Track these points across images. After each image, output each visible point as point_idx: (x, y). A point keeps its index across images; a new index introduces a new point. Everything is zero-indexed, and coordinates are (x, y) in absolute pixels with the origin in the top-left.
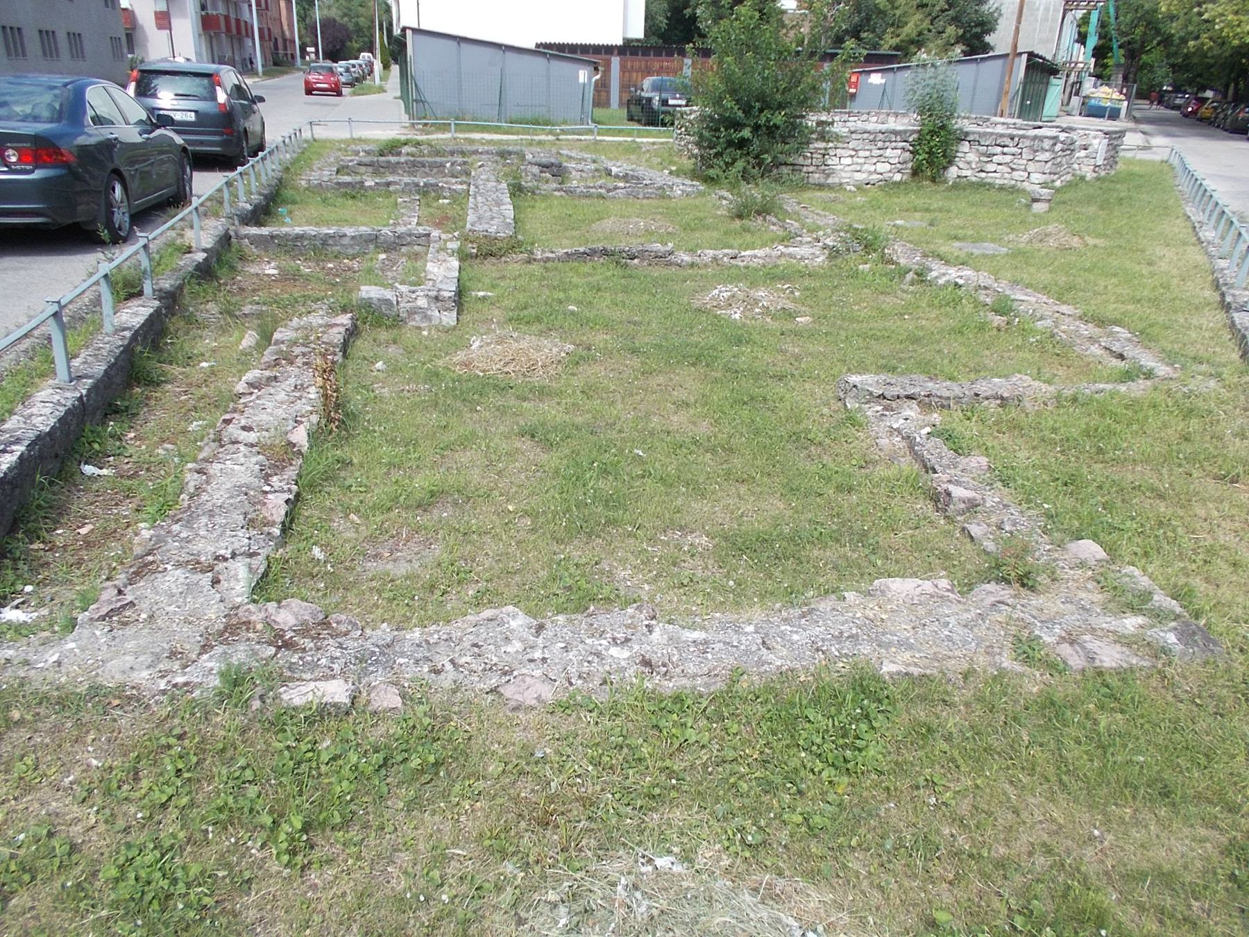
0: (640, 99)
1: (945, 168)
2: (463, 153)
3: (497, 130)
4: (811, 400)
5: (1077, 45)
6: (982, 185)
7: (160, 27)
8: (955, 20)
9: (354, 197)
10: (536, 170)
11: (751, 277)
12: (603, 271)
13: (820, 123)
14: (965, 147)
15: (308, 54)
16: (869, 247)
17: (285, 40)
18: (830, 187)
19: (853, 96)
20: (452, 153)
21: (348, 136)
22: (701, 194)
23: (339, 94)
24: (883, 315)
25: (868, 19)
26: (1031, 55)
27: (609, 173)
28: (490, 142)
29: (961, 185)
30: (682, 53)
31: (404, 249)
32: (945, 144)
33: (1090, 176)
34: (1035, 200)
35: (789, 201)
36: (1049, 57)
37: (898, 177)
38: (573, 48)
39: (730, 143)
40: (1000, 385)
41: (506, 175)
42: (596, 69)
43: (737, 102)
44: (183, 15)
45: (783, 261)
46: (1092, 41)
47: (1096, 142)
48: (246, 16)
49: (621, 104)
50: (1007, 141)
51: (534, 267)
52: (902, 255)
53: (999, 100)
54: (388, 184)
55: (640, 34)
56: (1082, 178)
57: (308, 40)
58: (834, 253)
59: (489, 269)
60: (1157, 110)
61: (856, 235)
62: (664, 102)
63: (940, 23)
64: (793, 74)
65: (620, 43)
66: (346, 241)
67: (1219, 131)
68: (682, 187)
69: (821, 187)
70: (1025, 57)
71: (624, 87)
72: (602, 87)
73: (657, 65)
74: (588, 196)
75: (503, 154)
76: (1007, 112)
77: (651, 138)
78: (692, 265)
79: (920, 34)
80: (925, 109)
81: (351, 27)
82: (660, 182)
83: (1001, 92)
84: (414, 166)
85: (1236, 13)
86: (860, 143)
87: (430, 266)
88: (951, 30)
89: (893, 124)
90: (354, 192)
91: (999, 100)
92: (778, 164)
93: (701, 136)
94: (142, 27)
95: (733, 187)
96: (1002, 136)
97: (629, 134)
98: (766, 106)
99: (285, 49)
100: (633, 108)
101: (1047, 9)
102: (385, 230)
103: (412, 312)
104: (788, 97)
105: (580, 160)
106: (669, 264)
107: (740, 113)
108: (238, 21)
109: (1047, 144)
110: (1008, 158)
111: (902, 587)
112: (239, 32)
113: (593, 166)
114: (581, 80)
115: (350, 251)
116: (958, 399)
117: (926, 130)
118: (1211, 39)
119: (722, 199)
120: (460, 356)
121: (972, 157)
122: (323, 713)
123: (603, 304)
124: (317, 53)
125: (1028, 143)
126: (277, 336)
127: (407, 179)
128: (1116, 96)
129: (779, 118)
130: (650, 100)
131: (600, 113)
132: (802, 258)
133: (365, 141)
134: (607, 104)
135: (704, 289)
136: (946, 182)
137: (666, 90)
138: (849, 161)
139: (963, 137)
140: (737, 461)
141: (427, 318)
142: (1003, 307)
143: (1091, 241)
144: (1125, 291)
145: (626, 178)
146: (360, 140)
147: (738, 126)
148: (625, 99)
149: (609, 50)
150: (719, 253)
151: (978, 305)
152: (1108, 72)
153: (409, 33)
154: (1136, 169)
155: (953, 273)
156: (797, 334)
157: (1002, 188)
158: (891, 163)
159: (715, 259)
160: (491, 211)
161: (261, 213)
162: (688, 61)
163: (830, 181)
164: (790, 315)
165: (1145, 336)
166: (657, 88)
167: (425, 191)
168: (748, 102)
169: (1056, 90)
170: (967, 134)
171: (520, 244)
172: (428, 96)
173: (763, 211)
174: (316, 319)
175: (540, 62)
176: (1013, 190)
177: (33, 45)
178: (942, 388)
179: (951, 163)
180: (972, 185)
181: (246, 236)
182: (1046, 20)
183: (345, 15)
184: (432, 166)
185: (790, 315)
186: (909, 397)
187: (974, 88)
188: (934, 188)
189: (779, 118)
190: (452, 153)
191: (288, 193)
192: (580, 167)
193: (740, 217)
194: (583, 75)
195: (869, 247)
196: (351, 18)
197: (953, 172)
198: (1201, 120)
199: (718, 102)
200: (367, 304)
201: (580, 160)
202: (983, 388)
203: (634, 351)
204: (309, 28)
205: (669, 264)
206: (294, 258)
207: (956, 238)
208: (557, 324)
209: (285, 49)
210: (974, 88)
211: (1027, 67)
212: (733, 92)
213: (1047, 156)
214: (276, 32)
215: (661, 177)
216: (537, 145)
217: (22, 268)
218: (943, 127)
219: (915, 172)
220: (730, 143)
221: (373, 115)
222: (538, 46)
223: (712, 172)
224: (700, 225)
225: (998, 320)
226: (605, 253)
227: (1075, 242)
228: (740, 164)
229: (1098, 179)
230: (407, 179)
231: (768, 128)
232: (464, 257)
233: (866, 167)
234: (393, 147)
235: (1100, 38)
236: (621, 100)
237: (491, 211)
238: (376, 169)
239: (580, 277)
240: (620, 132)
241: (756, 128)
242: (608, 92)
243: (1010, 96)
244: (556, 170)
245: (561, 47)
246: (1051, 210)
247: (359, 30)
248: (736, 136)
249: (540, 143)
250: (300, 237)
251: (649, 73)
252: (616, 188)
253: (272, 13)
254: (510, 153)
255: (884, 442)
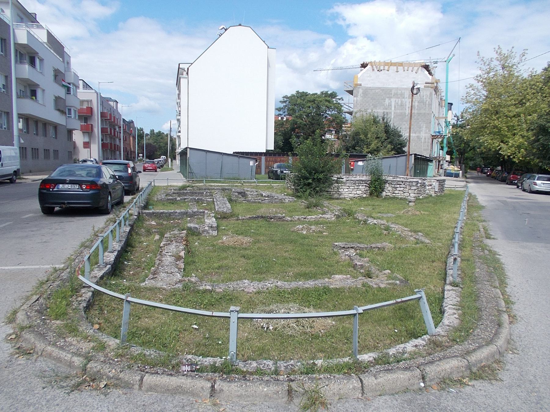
0: (273, 171)
1: (381, 192)
2: (209, 189)
3: (220, 182)
4: (325, 251)
5: (441, 151)
6: (394, 198)
7: (85, 147)
8: (391, 143)
9: (173, 204)
10: (236, 194)
11: (310, 223)
12: (261, 222)
13: (338, 178)
14: (387, 185)
15: (140, 156)
16: (349, 215)
17: (131, 152)
18: (341, 199)
19: (352, 169)
20: (205, 189)
21: (166, 185)
22: (295, 201)
23: (156, 171)
24: (352, 232)
25: (358, 143)
26: (415, 155)
27: (262, 195)
28: (220, 186)
29: (387, 198)
30: (288, 156)
31: (196, 217)
32: (380, 184)
33: (433, 195)
34: (410, 202)
35: (326, 203)
36: (428, 156)
37: (365, 196)
38: (247, 153)
39: (305, 185)
40: (379, 245)
41: (226, 196)
42: (256, 161)
43: (307, 171)
44: (95, 143)
45: (321, 219)
46: (446, 149)
47: (434, 183)
48: (118, 143)
49: (265, 173)
50: (401, 183)
51: (239, 221)
52: (360, 216)
53: (406, 170)
54: (185, 199)
55: (271, 147)
56: (431, 196)
57: (140, 151)
58: (338, 217)
59: (224, 222)
60: (475, 173)
61: (344, 210)
62: (282, 172)
63: (385, 144)
64: (325, 161)
65: (265, 151)
66: (176, 214)
67: (497, 181)
68: (288, 199)
69: (337, 199)
70: (413, 155)
71: (267, 167)
72: (259, 167)
73: (279, 159)
74: (255, 202)
75: (224, 190)
76: (409, 174)
77: (277, 184)
78: (291, 221)
79: (378, 147)
80: (372, 173)
81: (157, 146)
82: (280, 197)
83: (406, 168)
84: (192, 194)
85: (492, 140)
86: (351, 186)
87: (206, 220)
88: (389, 146)
89: (364, 178)
90: (173, 202)
91: (406, 170)
92: (321, 191)
93: (295, 182)
94: (78, 147)
95: (306, 199)
96: (399, 181)
97: (269, 182)
98: (317, 172)
99: (131, 155)
100: (270, 174)
101: (425, 139)
102: (189, 211)
103: (204, 231)
104: (324, 169)
105: (251, 192)
106: (284, 221)
107: (308, 174)
108: (115, 145)
109: (414, 184)
110: (402, 189)
111: (337, 277)
112: (115, 149)
113: (256, 193)
114: (251, 165)
115: (178, 217)
116: (366, 248)
117: (373, 180)
118: (484, 148)
119: (302, 203)
120: (220, 241)
121: (390, 188)
122: (205, 291)
123: (263, 230)
124: (143, 156)
125: (408, 183)
126: (165, 236)
127: (191, 197)
128: (456, 169)
129: (321, 176)
130: (277, 171)
131: (257, 176)
132: (328, 218)
133: (174, 186)
134: (260, 173)
135: (295, 226)
136: (382, 197)
137: (282, 168)
138: (347, 190)
139: (386, 182)
140: (301, 261)
141: (208, 233)
142: (387, 229)
143: (422, 212)
144: (428, 224)
145: (268, 196)
146: (171, 186)
147: (307, 179)
148: (267, 172)
149: (261, 154)
150: (300, 217)
151: (380, 228)
152: (454, 160)
153: (188, 149)
154: (453, 193)
155: (375, 221)
156: (323, 237)
157: (401, 199)
158: (362, 191)
159: (299, 219)
160: (223, 205)
161: (146, 207)
162: (290, 158)
163: (341, 197)
164: (321, 232)
165: (427, 235)
166: (279, 167)
167: (197, 201)
168: (310, 171)
169: (432, 168)
170: (387, 181)
171: (234, 215)
172: (195, 170)
173: (316, 206)
174: (176, 232)
175: (236, 158)
176: (405, 199)
177: (41, 154)
178: (362, 246)
179: (383, 191)
180: (391, 198)
181: (145, 213)
182: (425, 142)
183: (155, 142)
184: (199, 193)
185: (321, 232)
186: (352, 248)
187: (396, 166)
188: (378, 199)
189: (321, 176)
190: (205, 189)
191: (151, 202)
192: (251, 193)
193: (308, 208)
194: (252, 163)
195: (349, 215)
196: (157, 143)
197: (384, 194)
198: (493, 177)
199: (300, 171)
200: (190, 229)
201: (251, 192)
202: (373, 246)
203: (272, 241)
204: (141, 147)
205: (284, 221)
206: (160, 220)
207: (380, 213)
208: (248, 235)
209: (131, 155)
210: (396, 166)
211: (415, 159)
212: (305, 168)
213: (415, 188)
214: (128, 149)
215: (281, 196)
216: (237, 187)
217: (27, 237)
218: (379, 179)
219: (371, 194)
220: (305, 185)
221: (170, 178)
222: (234, 153)
223: (299, 194)
224: (295, 210)
225: (385, 232)
226: (262, 217)
227: (418, 213)
228: (308, 191)
229: (437, 196)
230: (191, 197)
231: (318, 179)
232: (217, 219)
233: (353, 192)
234: (184, 188)
235: (449, 147)
236: (265, 171)
237: (223, 205)
238: (179, 195)
239: (254, 224)
240: (265, 182)
241: (314, 179)
242: (261, 169)
243: (410, 169)
244: (243, 194)
245: (243, 153)
246: (416, 204)
247: (160, 147)
248: (307, 182)
249: (236, 186)
250: (162, 213)
251: (276, 162)
252: (265, 200)
253: (127, 142)
254: (226, 189)
255: (343, 257)
